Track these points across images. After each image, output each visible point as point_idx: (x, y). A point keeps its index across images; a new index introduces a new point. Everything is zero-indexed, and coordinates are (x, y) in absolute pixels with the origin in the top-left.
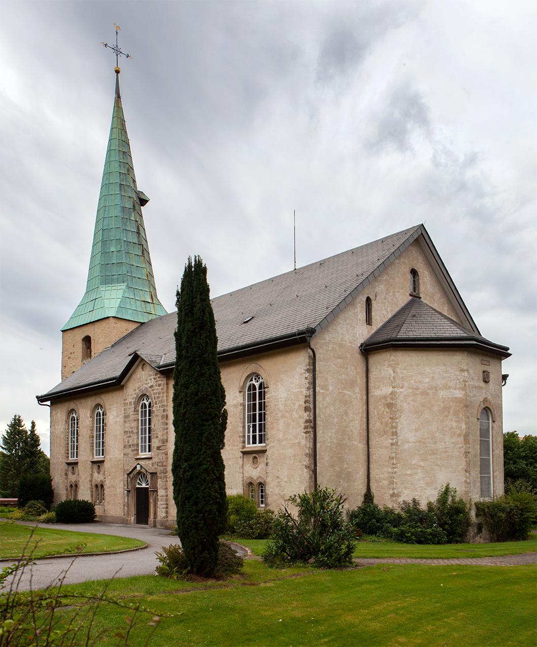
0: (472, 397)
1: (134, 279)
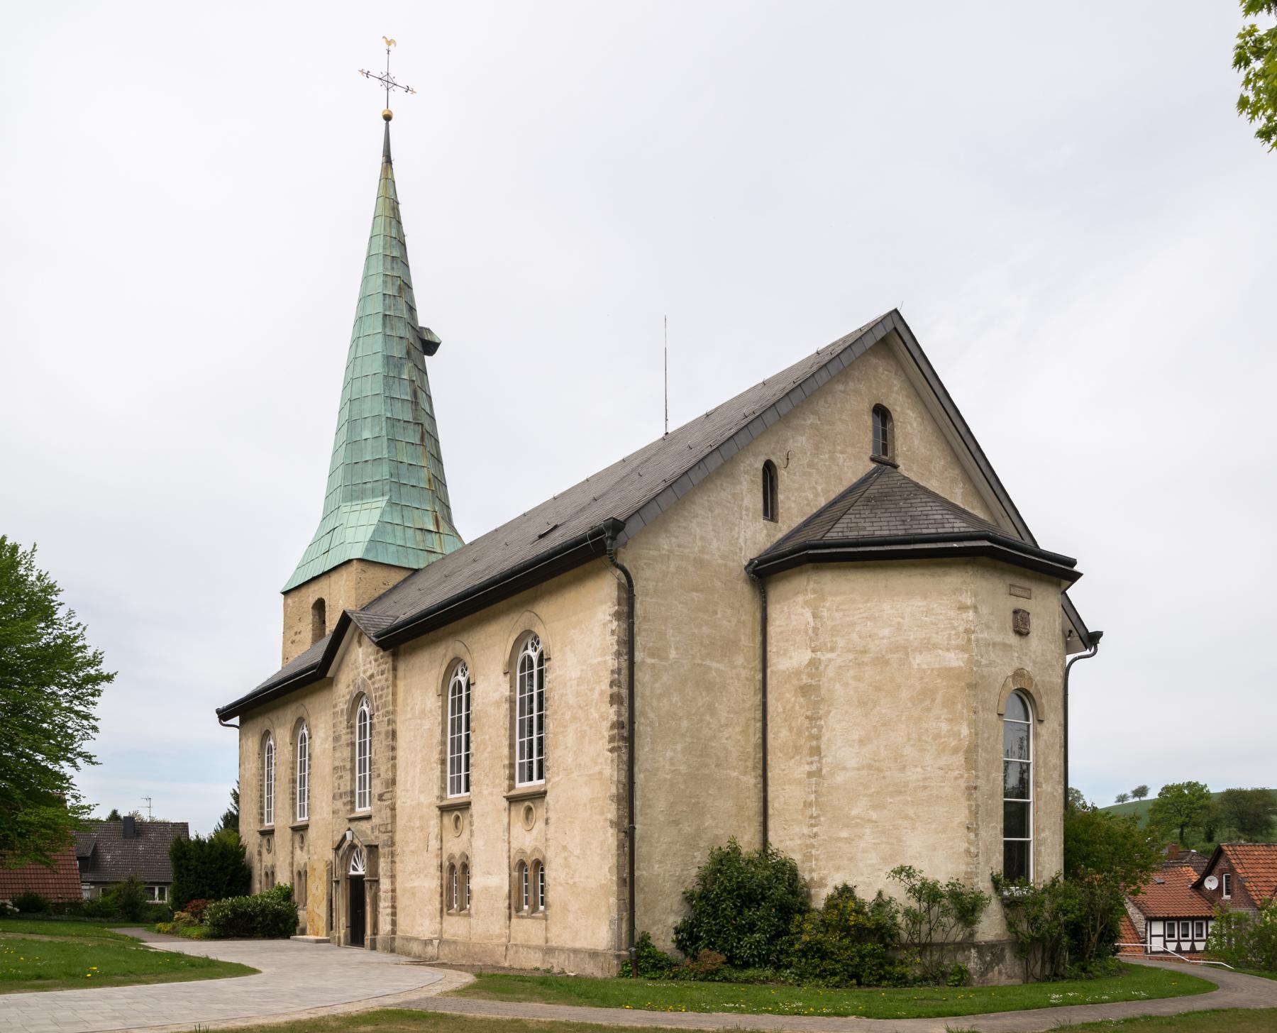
0: (987, 666)
1: (404, 490)
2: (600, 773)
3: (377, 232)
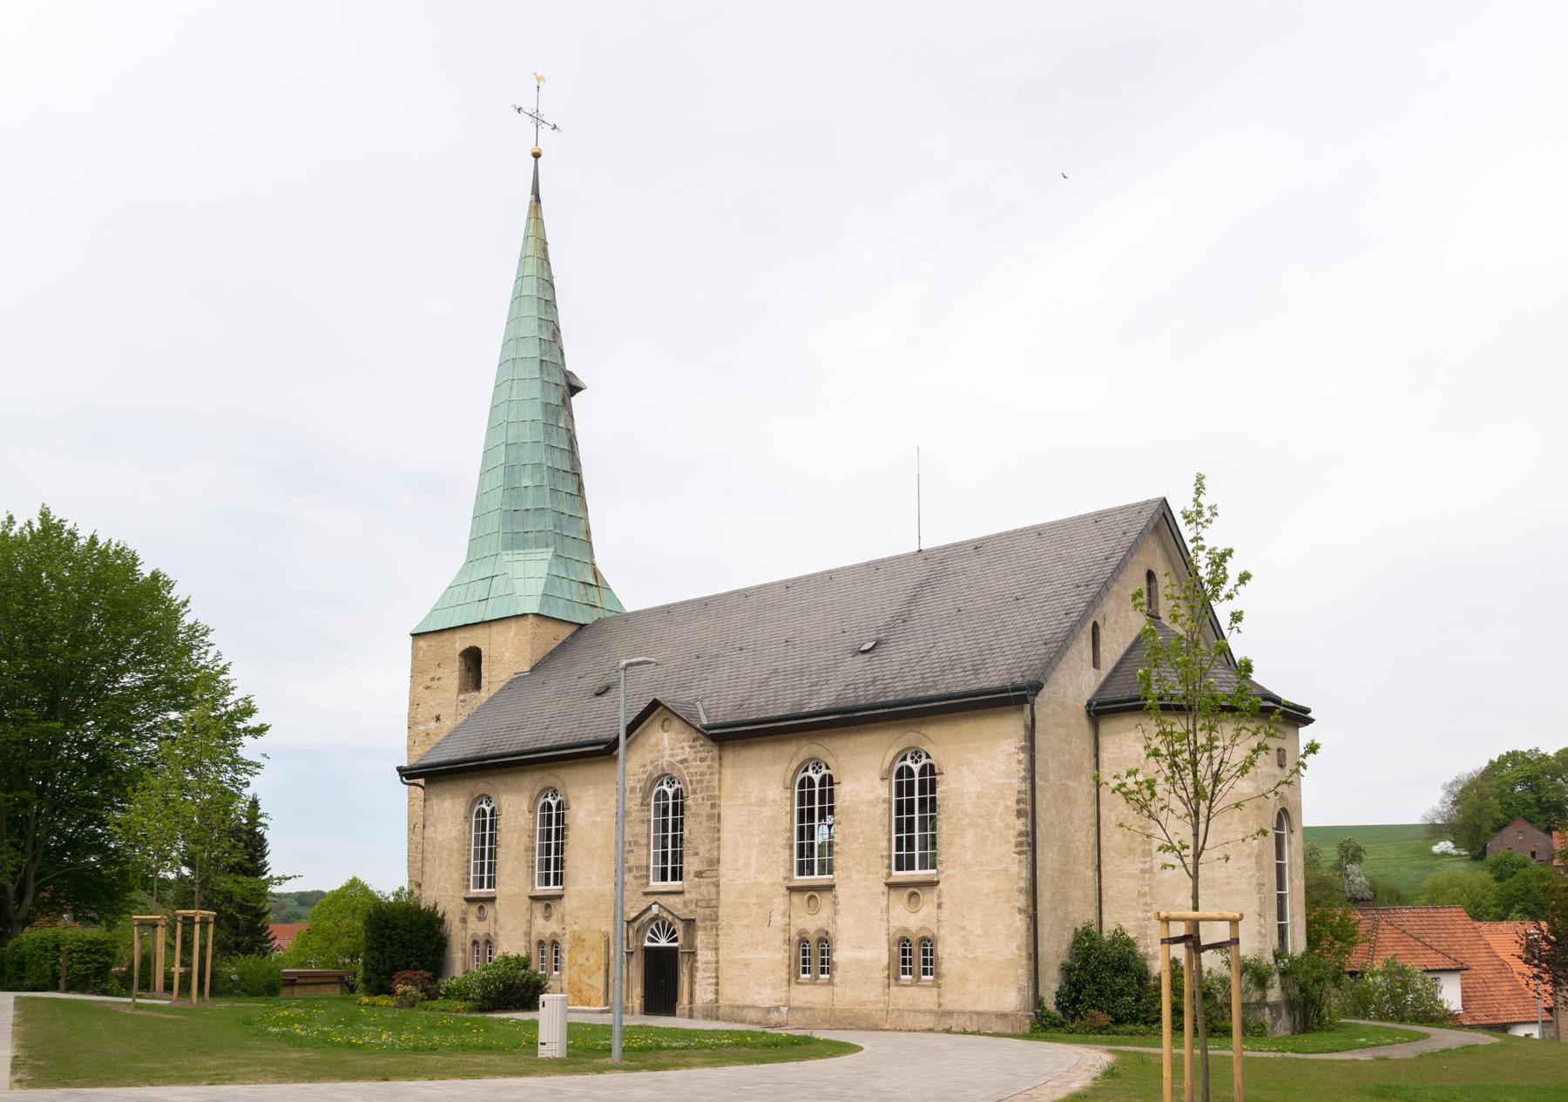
1: (567, 541)
2: (1006, 870)
3: (528, 271)
